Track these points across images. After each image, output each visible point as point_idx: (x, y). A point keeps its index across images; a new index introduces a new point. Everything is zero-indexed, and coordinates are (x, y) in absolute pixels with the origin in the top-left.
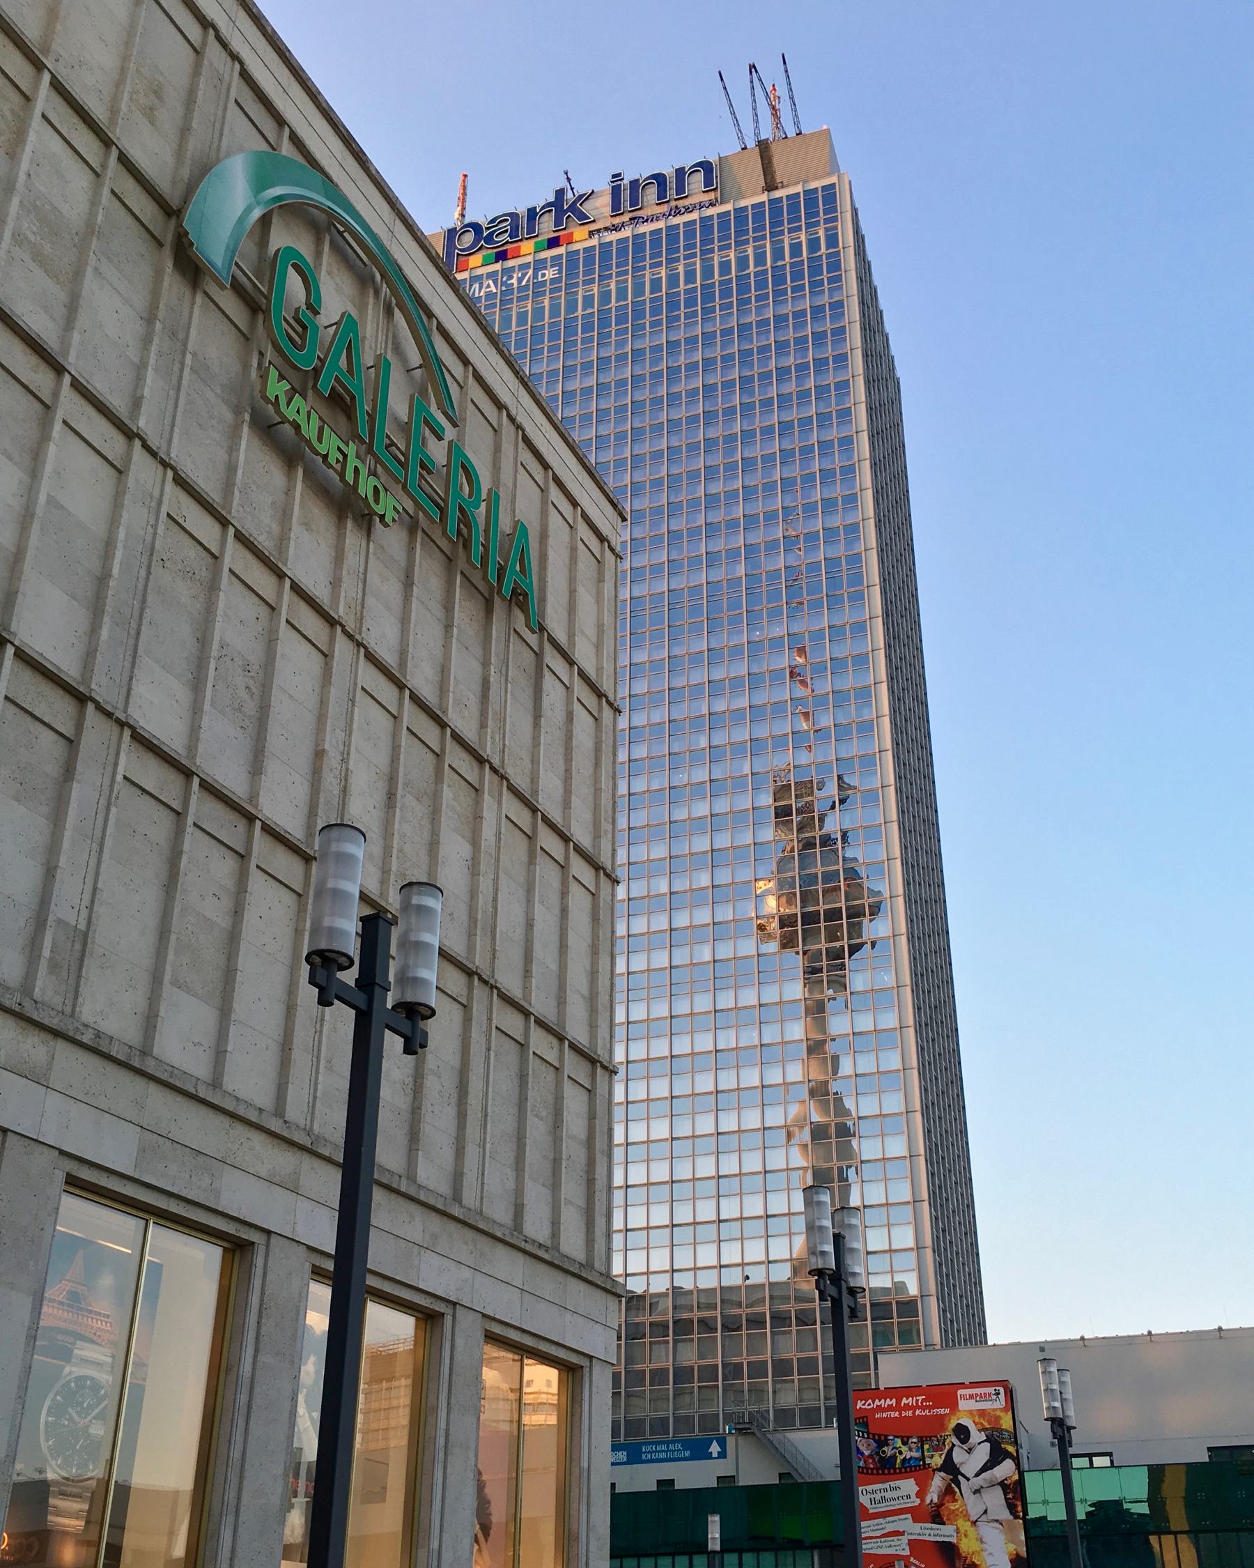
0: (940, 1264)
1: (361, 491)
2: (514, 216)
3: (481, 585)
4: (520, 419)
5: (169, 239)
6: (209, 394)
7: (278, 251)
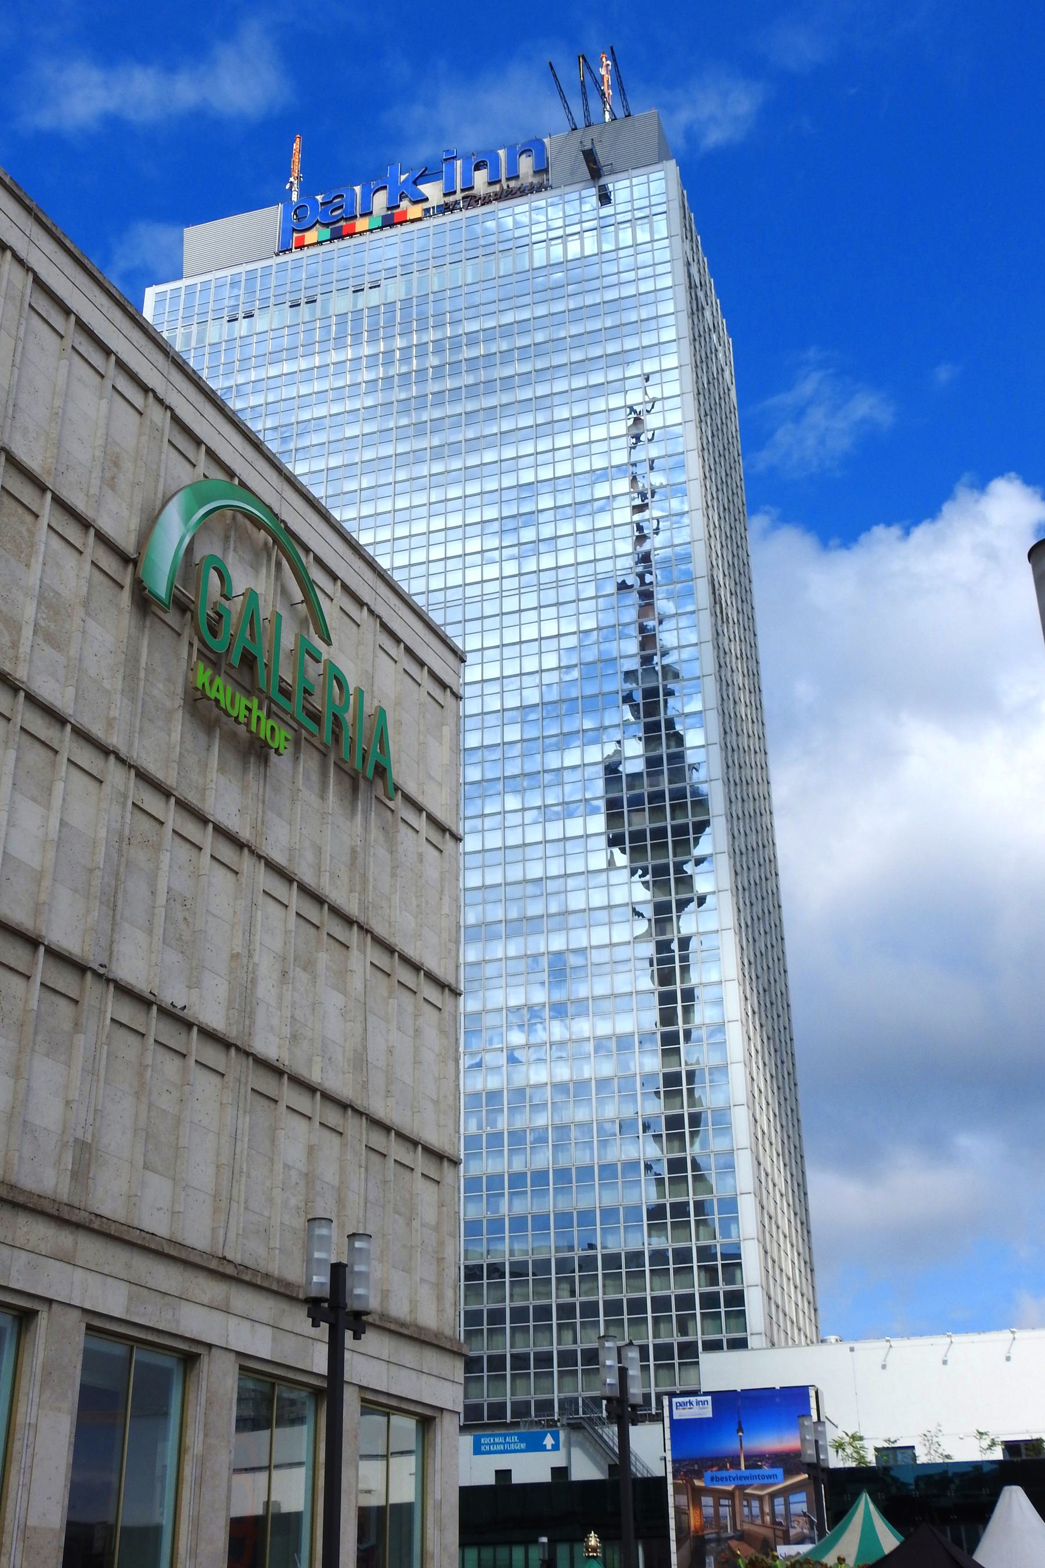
7: (203, 558)
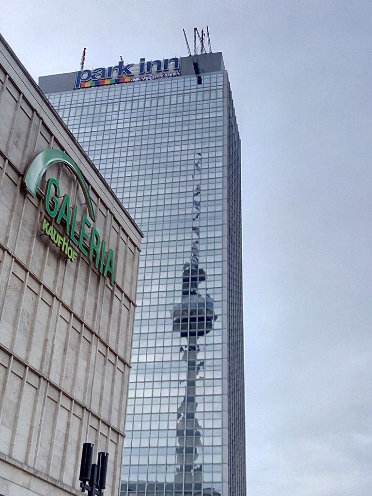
0: (231, 488)
1: (66, 253)
2: (103, 69)
3: (97, 273)
4: (113, 212)
5: (19, 184)
6: (25, 229)
7: (49, 180)
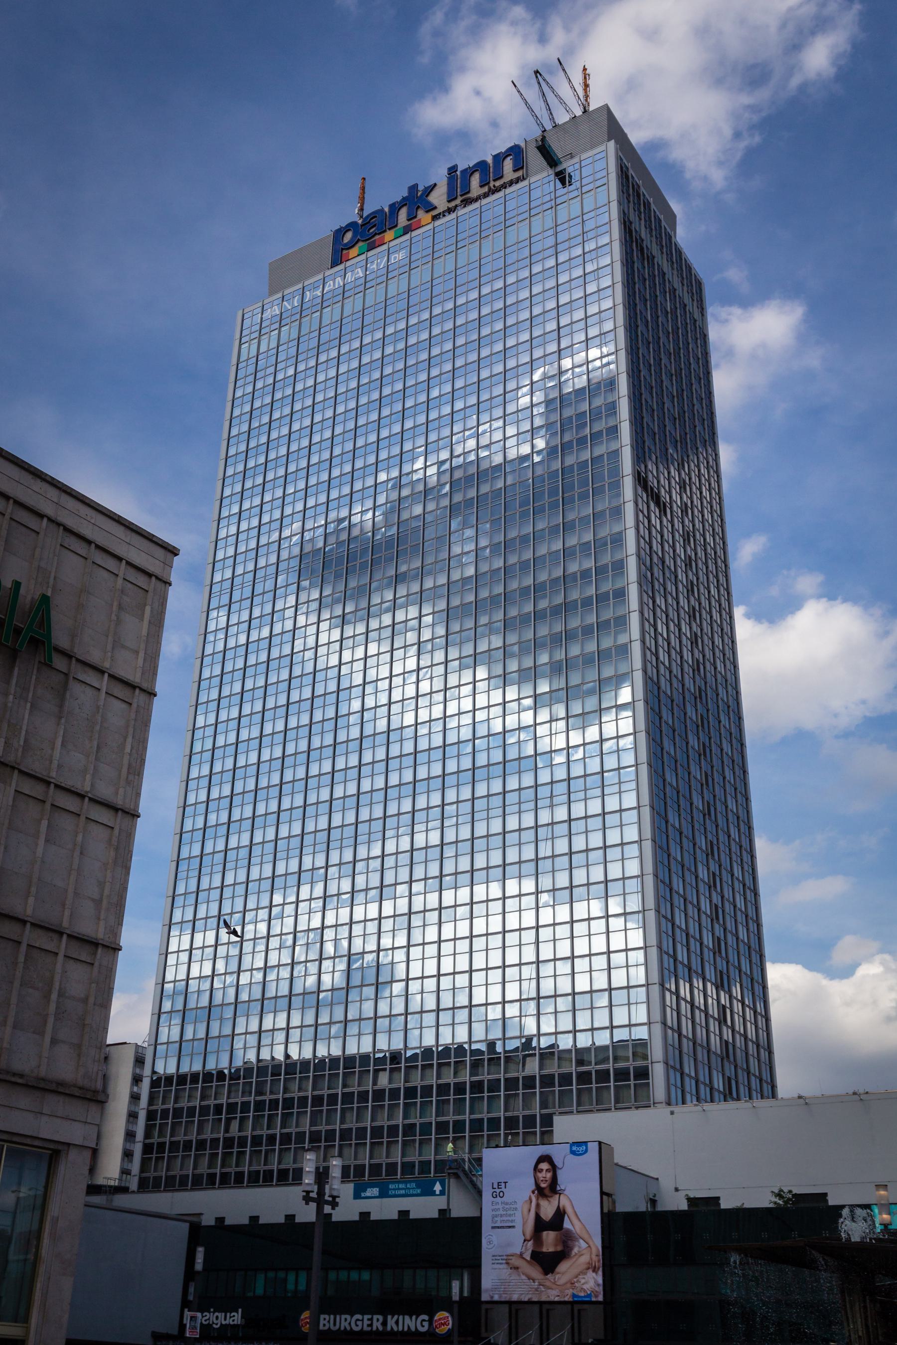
2: (382, 210)
